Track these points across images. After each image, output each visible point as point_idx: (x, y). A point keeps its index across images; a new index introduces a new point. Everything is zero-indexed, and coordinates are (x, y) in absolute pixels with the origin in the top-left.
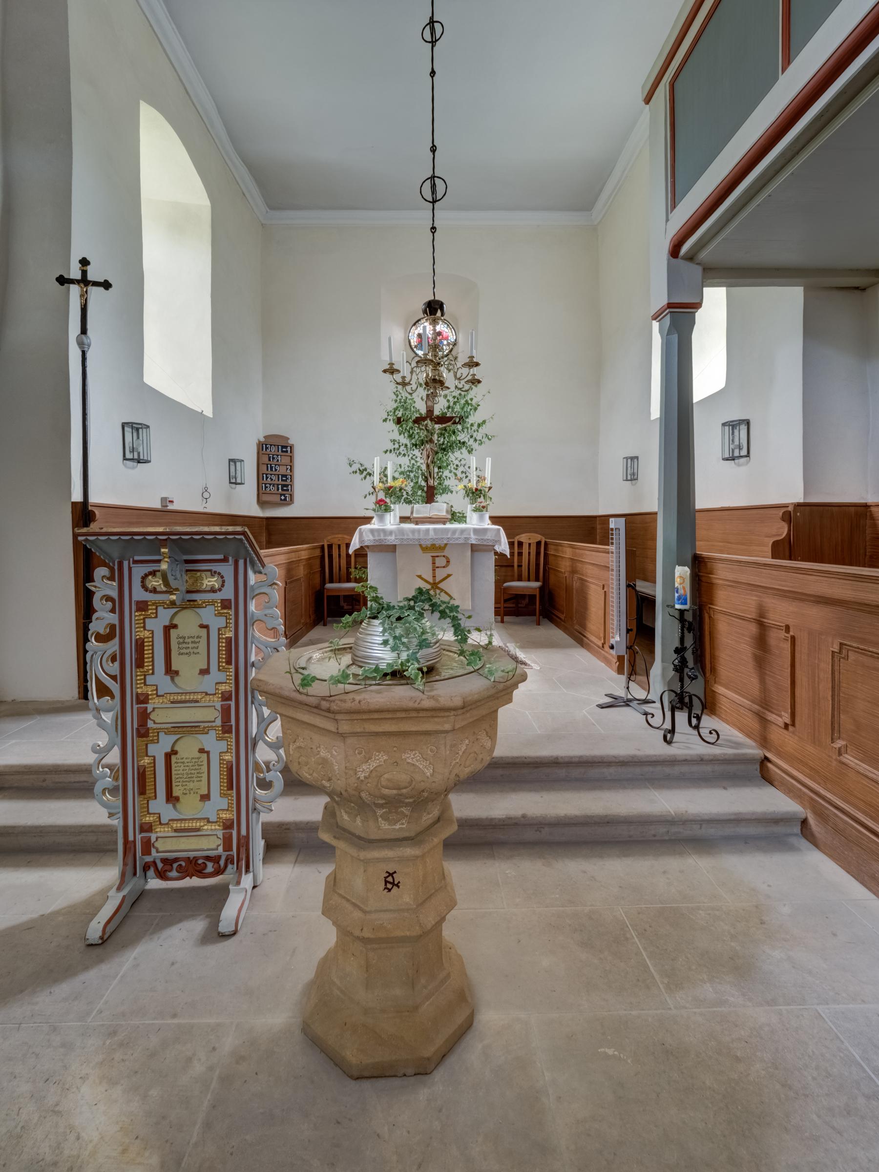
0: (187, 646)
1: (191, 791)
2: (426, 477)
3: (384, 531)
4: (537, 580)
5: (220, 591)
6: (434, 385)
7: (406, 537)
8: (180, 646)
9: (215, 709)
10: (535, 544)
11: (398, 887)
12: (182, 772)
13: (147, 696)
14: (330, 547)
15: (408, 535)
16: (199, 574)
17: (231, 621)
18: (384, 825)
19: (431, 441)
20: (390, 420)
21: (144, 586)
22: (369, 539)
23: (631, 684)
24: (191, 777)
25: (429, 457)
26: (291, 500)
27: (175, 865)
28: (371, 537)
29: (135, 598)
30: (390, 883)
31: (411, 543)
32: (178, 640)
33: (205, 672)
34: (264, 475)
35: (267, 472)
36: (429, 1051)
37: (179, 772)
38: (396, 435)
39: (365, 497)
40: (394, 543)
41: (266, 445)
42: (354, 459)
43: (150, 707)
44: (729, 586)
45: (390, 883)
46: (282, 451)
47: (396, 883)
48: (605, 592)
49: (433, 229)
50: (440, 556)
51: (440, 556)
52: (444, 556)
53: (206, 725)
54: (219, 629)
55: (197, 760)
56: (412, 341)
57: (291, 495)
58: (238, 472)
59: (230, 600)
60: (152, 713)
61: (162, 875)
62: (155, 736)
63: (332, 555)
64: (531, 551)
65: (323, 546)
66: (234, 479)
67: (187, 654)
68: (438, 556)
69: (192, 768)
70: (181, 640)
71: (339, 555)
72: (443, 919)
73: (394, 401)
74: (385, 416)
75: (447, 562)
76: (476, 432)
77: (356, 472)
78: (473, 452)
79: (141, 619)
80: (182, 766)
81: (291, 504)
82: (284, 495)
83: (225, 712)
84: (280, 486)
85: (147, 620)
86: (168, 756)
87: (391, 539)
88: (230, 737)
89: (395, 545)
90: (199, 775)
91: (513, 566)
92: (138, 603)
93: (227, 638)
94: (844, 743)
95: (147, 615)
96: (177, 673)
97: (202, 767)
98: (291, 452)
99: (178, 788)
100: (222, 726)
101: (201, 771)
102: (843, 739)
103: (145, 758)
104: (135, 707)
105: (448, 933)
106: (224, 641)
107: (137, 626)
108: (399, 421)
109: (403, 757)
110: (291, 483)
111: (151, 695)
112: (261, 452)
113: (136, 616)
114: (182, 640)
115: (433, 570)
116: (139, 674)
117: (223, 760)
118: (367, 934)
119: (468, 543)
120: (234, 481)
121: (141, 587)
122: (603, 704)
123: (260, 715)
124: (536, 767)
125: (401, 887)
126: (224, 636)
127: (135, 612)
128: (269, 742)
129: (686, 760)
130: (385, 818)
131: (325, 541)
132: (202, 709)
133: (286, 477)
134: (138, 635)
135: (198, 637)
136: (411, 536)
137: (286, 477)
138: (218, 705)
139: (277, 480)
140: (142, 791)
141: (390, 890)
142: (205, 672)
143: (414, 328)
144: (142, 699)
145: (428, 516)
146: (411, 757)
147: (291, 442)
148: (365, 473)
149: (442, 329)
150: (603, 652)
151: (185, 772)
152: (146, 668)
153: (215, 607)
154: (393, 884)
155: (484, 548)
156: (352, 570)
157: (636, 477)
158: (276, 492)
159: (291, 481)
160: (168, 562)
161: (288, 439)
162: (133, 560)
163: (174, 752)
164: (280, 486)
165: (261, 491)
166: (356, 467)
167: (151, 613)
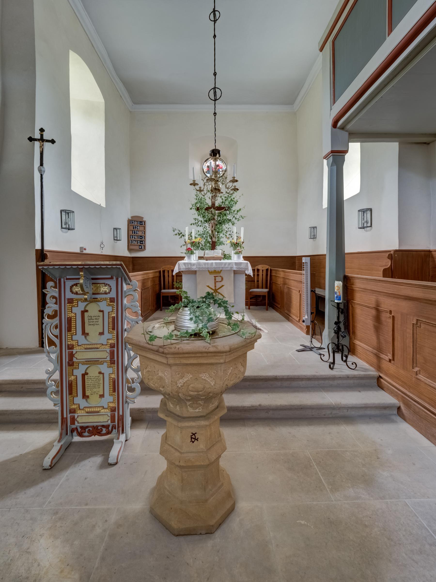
0: (93, 321)
1: (95, 393)
2: (211, 237)
3: (190, 264)
4: (266, 288)
5: (109, 294)
6: (215, 191)
7: (201, 267)
8: (89, 321)
9: (107, 352)
10: (266, 270)
11: (198, 440)
12: (90, 383)
13: (73, 345)
14: (164, 271)
15: (202, 266)
16: (98, 285)
17: (114, 309)
18: (191, 410)
19: (214, 219)
20: (193, 209)
21: (71, 291)
22: (183, 268)
23: (313, 340)
24: (95, 386)
25: (213, 227)
26: (144, 248)
27: (87, 430)
28: (184, 267)
29: (67, 297)
30: (193, 438)
31: (204, 270)
32: (88, 318)
33: (102, 334)
34: (131, 236)
35: (132, 235)
36: (213, 522)
37: (89, 383)
38: (196, 216)
39: (181, 247)
40: (195, 270)
41: (132, 221)
42: (176, 228)
43: (74, 351)
44: (361, 291)
45: (193, 438)
46: (140, 224)
47: (196, 438)
48: (300, 294)
49: (215, 114)
50: (218, 276)
51: (218, 276)
52: (220, 276)
53: (102, 360)
54: (109, 313)
55: (98, 378)
56: (204, 169)
57: (144, 246)
58: (118, 234)
59: (114, 298)
60: (75, 354)
61: (80, 435)
62: (77, 366)
63: (165, 275)
64: (263, 274)
65: (160, 271)
66: (116, 238)
67: (93, 325)
68: (217, 276)
69: (95, 381)
70: (90, 318)
71: (168, 276)
72: (220, 456)
73: (195, 199)
74: (191, 207)
75: (222, 279)
76: (236, 215)
77: (177, 234)
78: (235, 224)
79: (70, 308)
80: (90, 381)
81: (144, 250)
82: (141, 246)
83: (112, 354)
84: (139, 241)
85: (73, 308)
86: (83, 376)
87: (194, 268)
88: (114, 366)
89: (196, 271)
90: (99, 385)
91: (254, 281)
92: (68, 299)
93: (112, 317)
94: (418, 369)
95: (73, 305)
96: (88, 334)
97: (100, 381)
98: (144, 224)
99: (88, 391)
100: (110, 360)
101: (100, 383)
102: (418, 367)
103: (72, 376)
104: (67, 351)
105: (222, 463)
106: (111, 318)
107: (68, 311)
108: (198, 209)
109: (200, 376)
110: (144, 240)
111: (75, 345)
112: (129, 224)
113: (67, 306)
114: (90, 318)
115: (215, 283)
116: (69, 334)
117: (111, 377)
118: (182, 464)
119: (232, 270)
120: (116, 239)
121: (70, 292)
122: (299, 350)
123: (129, 355)
124: (266, 381)
125: (199, 440)
126: (111, 316)
127: (67, 304)
128: (134, 368)
129: (340, 378)
130: (191, 406)
131: (161, 269)
132: (100, 352)
133: (142, 237)
134: (68, 315)
135: (98, 316)
136: (204, 266)
137: (142, 237)
138: (108, 350)
139: (137, 238)
140: (71, 393)
141: (193, 442)
142: (102, 334)
143: (205, 163)
144: (71, 347)
145: (212, 256)
146: (204, 376)
147: (144, 219)
148: (181, 235)
149: (219, 163)
150: (299, 324)
151: (92, 383)
152: (73, 332)
153: (107, 301)
154: (195, 439)
155: (240, 272)
156: (175, 283)
157: (315, 237)
158: (137, 244)
159: (144, 239)
160: (83, 279)
161: (143, 218)
162: (66, 278)
163: (86, 374)
164: (139, 241)
165: (129, 244)
166: (176, 232)
167: (75, 304)
